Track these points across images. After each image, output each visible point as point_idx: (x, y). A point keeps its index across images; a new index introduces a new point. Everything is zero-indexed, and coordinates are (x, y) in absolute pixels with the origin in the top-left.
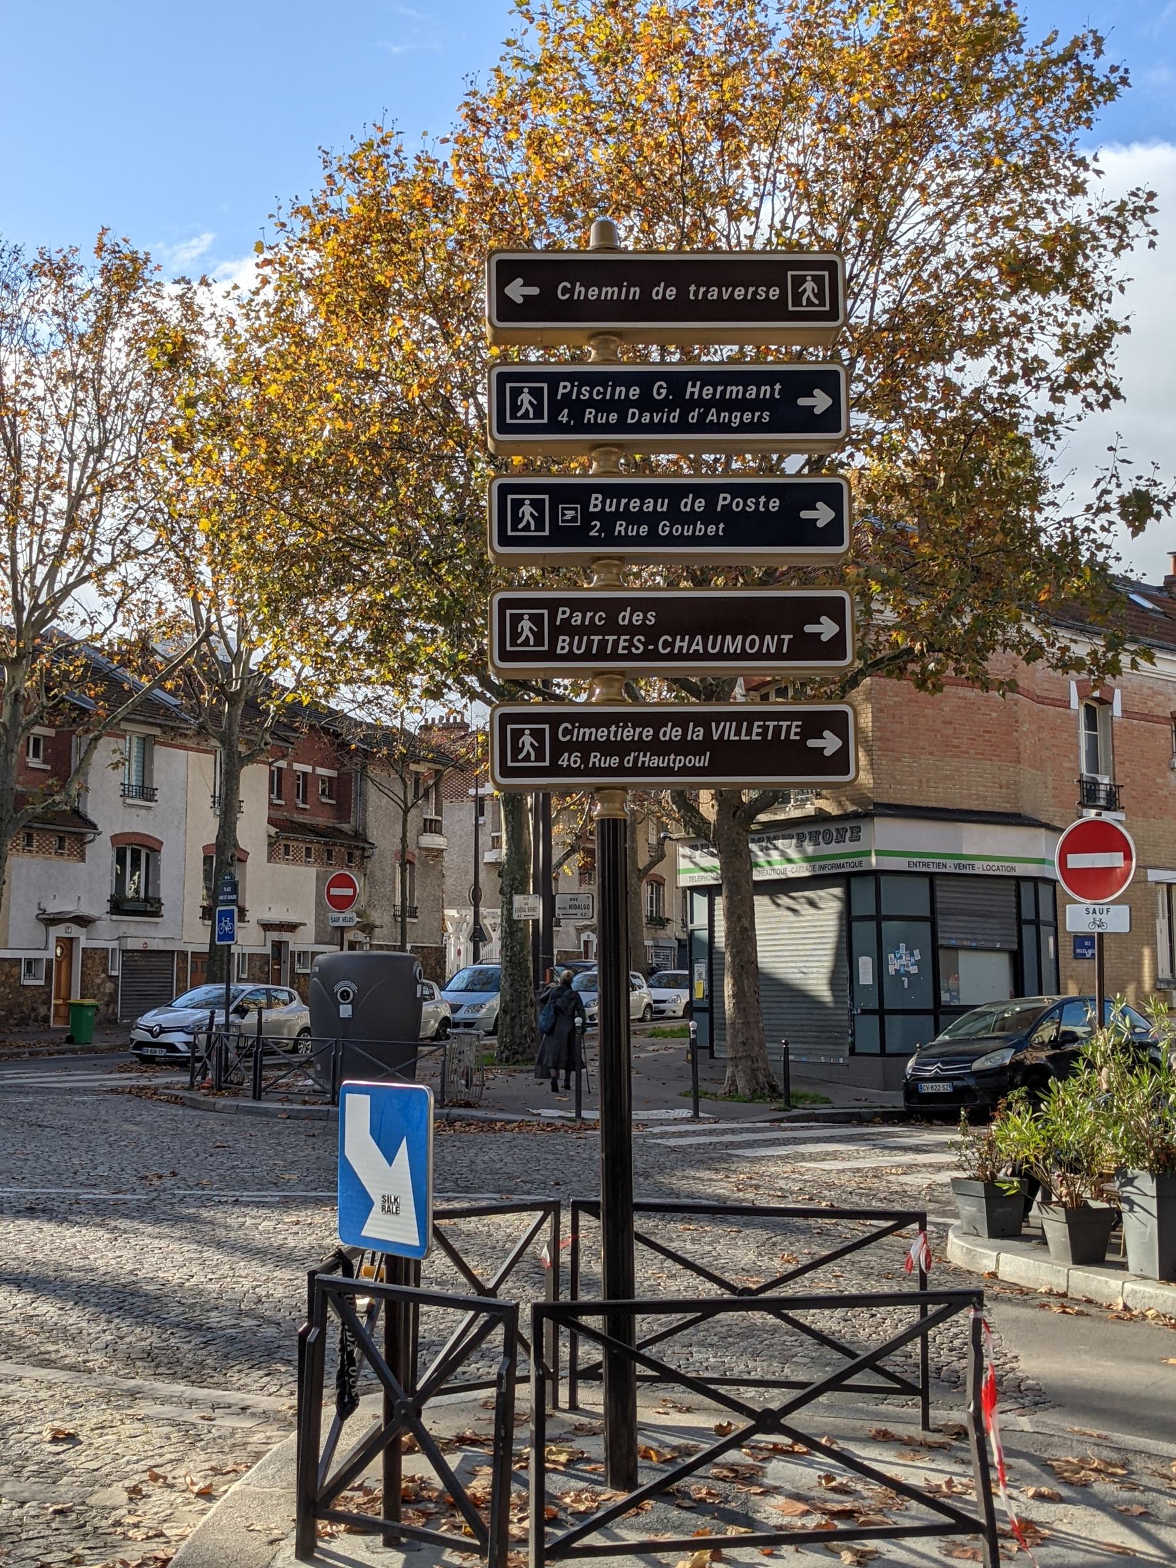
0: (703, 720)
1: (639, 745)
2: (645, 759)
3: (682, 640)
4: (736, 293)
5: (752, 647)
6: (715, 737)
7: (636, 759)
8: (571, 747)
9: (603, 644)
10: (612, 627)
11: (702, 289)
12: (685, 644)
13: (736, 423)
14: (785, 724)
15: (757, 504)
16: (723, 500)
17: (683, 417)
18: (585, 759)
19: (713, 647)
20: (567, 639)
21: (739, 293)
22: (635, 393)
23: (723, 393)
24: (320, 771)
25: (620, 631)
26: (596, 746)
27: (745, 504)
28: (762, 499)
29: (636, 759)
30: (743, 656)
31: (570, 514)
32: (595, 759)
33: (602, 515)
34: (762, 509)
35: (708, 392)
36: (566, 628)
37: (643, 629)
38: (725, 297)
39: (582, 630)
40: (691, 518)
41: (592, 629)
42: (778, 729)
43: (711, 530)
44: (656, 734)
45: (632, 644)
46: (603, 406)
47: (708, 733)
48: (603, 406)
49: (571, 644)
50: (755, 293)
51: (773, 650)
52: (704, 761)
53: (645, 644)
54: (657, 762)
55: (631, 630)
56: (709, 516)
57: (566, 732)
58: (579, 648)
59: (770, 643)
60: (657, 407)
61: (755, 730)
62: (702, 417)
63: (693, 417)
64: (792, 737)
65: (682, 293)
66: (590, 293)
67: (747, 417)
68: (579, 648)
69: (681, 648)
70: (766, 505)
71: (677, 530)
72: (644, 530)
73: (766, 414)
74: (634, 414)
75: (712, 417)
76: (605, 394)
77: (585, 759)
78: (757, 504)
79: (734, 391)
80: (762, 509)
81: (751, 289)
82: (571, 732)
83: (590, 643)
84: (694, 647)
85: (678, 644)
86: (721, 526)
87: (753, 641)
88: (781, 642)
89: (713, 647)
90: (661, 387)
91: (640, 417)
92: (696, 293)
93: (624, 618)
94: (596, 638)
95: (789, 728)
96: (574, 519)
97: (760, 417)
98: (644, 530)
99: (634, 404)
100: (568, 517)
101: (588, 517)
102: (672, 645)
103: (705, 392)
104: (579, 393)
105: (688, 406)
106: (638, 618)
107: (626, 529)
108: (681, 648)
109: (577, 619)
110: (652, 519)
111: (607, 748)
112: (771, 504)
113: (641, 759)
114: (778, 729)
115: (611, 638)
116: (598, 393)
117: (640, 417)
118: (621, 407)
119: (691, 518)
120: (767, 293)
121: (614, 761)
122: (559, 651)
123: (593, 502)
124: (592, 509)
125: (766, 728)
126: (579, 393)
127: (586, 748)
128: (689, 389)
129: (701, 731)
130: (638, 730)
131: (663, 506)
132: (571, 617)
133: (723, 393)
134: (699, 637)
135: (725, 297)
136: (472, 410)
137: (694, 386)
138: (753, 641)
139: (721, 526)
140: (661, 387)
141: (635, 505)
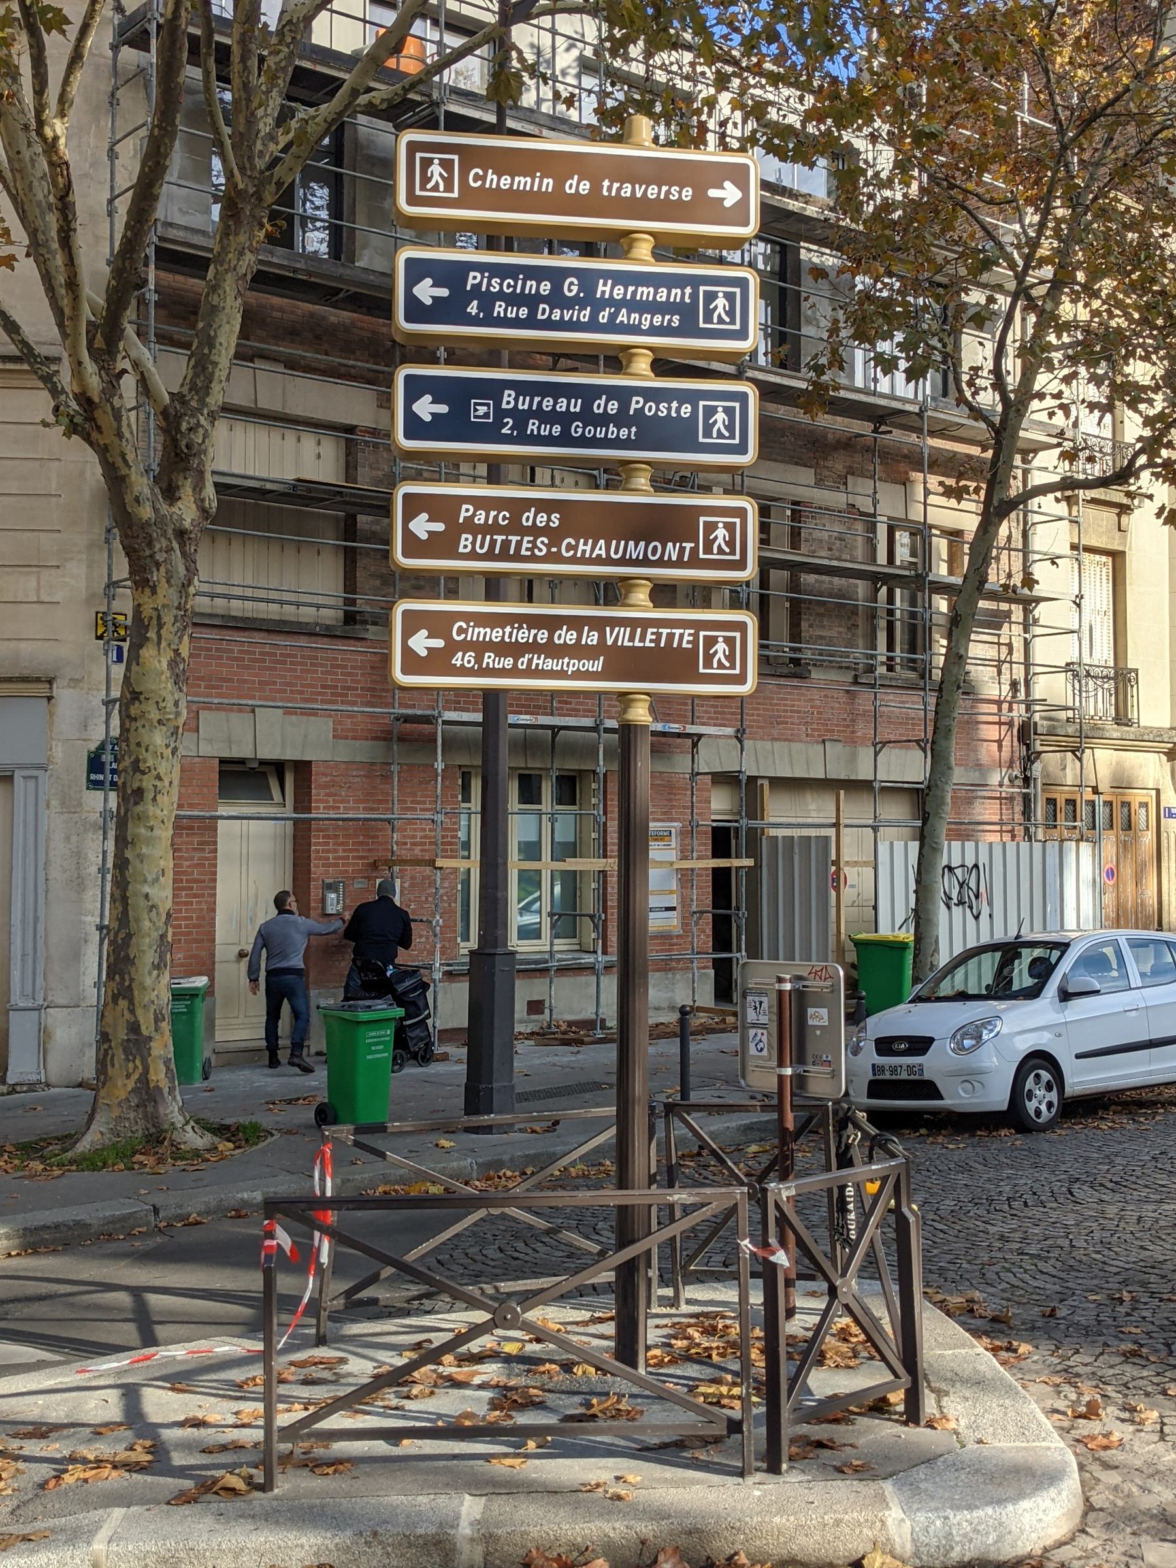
0: (599, 624)
1: (533, 647)
2: (539, 662)
3: (585, 544)
4: (650, 191)
5: (654, 554)
6: (610, 642)
7: (530, 661)
8: (466, 646)
9: (506, 544)
10: (515, 527)
11: (616, 185)
12: (588, 548)
13: (645, 325)
14: (678, 632)
15: (669, 409)
16: (636, 403)
17: (594, 316)
18: (479, 659)
19: (616, 552)
20: (470, 537)
21: (652, 192)
22: (546, 288)
23: (634, 293)
24: (440, 766)
25: (523, 531)
26: (490, 646)
27: (658, 409)
28: (675, 405)
29: (530, 661)
30: (645, 562)
31: (482, 410)
32: (489, 659)
33: (514, 412)
34: (674, 414)
35: (618, 293)
36: (470, 526)
37: (546, 531)
38: (639, 195)
39: (486, 529)
40: (604, 420)
41: (495, 528)
42: (671, 637)
43: (624, 433)
44: (551, 637)
45: (535, 546)
46: (514, 300)
47: (602, 637)
48: (514, 300)
49: (474, 543)
50: (668, 193)
51: (674, 558)
52: (597, 665)
53: (548, 546)
54: (550, 664)
55: (535, 531)
56: (621, 419)
57: (461, 631)
58: (482, 547)
59: (672, 551)
60: (568, 304)
61: (649, 637)
62: (612, 317)
63: (604, 317)
64: (685, 645)
65: (596, 187)
66: (502, 181)
67: (657, 320)
68: (482, 547)
69: (584, 552)
70: (678, 410)
71: (590, 431)
72: (557, 430)
73: (676, 318)
74: (544, 310)
75: (622, 317)
76: (515, 287)
77: (479, 659)
78: (669, 409)
79: (645, 292)
80: (674, 414)
81: (665, 188)
82: (465, 631)
83: (493, 543)
84: (597, 552)
85: (581, 547)
86: (634, 429)
87: (655, 548)
88: (682, 549)
89: (616, 552)
90: (572, 283)
91: (551, 313)
92: (610, 189)
93: (528, 518)
94: (499, 538)
95: (682, 636)
96: (486, 415)
97: (670, 321)
98: (557, 430)
99: (544, 299)
100: (480, 413)
101: (500, 413)
102: (575, 548)
103: (616, 291)
104: (489, 284)
105: (599, 305)
106: (542, 520)
107: (539, 428)
108: (584, 552)
109: (480, 518)
110: (566, 419)
111: (502, 649)
112: (683, 410)
113: (535, 661)
114: (671, 637)
115: (514, 539)
116: (509, 286)
117: (551, 313)
118: (532, 302)
119: (604, 420)
120: (680, 193)
121: (508, 663)
122: (461, 550)
123: (505, 399)
124: (504, 406)
125: (659, 635)
126: (489, 284)
127: (480, 648)
128: (600, 288)
129: (595, 636)
130: (533, 632)
131: (576, 407)
132: (474, 515)
133: (634, 293)
134: (602, 542)
135: (639, 195)
136: (65, 378)
137: (605, 285)
138: (655, 548)
139: (634, 429)
140: (572, 283)
141: (547, 404)
